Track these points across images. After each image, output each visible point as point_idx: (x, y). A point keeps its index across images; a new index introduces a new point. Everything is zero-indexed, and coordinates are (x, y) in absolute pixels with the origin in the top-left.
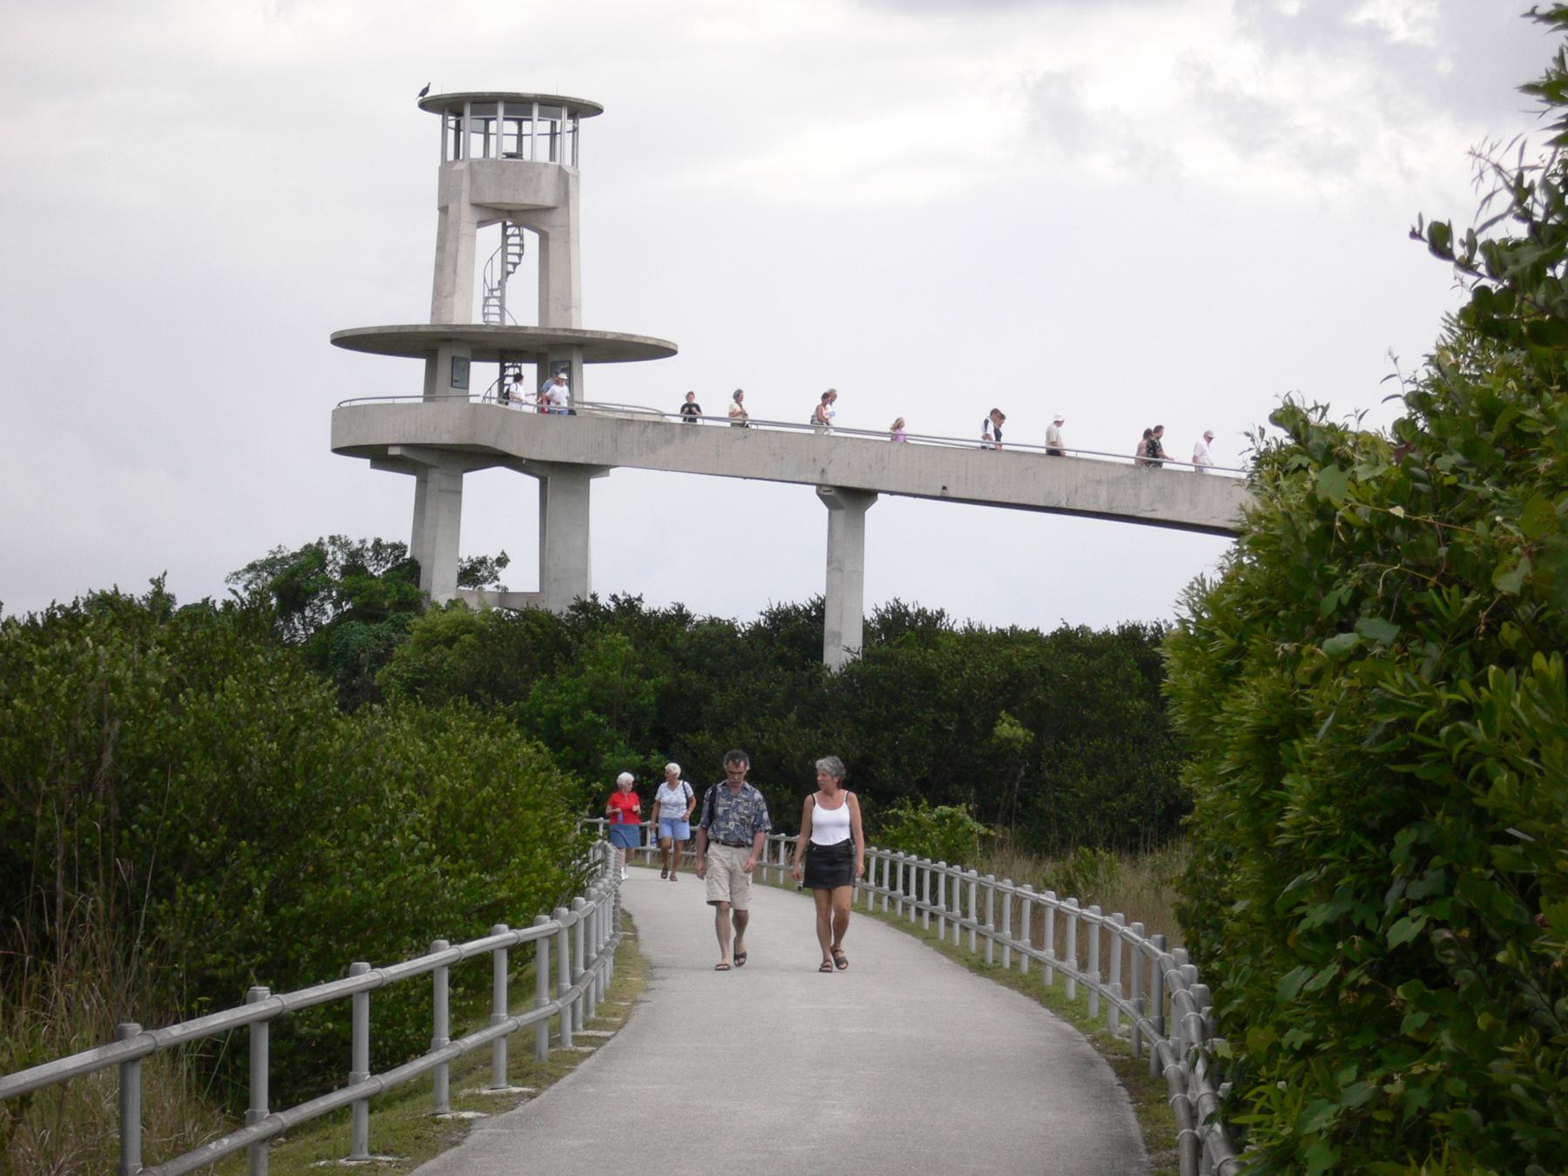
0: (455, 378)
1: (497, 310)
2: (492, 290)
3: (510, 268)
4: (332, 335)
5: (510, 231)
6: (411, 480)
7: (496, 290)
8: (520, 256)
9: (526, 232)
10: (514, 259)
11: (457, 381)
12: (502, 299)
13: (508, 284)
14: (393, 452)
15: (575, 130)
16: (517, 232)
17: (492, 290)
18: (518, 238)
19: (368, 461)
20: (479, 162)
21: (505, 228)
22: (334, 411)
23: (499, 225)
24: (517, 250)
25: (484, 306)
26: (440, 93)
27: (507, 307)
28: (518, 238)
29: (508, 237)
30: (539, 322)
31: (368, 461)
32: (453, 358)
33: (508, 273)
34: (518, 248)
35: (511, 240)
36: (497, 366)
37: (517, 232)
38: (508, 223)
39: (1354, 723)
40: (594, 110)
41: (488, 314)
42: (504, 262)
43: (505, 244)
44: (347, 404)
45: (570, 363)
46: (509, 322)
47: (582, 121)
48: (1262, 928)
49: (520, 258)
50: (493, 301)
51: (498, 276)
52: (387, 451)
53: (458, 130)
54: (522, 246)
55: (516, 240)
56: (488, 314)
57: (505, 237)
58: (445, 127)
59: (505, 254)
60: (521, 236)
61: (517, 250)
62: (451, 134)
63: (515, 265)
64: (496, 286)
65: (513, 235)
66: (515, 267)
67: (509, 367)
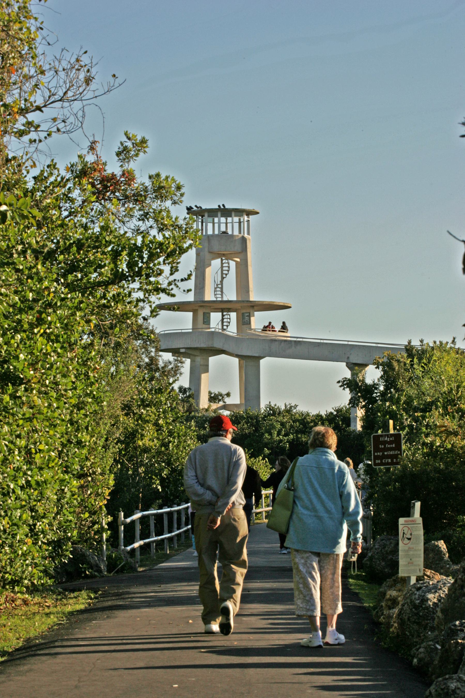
5: (224, 261)
8: (228, 271)
10: (226, 272)
12: (222, 288)
17: (217, 285)
21: (222, 260)
23: (220, 260)
24: (227, 268)
25: (215, 291)
33: (224, 278)
42: (222, 274)
43: (222, 267)
50: (218, 289)
51: (220, 279)
53: (202, 222)
54: (229, 267)
57: (222, 264)
59: (222, 270)
60: (228, 263)
63: (226, 274)
64: (219, 283)
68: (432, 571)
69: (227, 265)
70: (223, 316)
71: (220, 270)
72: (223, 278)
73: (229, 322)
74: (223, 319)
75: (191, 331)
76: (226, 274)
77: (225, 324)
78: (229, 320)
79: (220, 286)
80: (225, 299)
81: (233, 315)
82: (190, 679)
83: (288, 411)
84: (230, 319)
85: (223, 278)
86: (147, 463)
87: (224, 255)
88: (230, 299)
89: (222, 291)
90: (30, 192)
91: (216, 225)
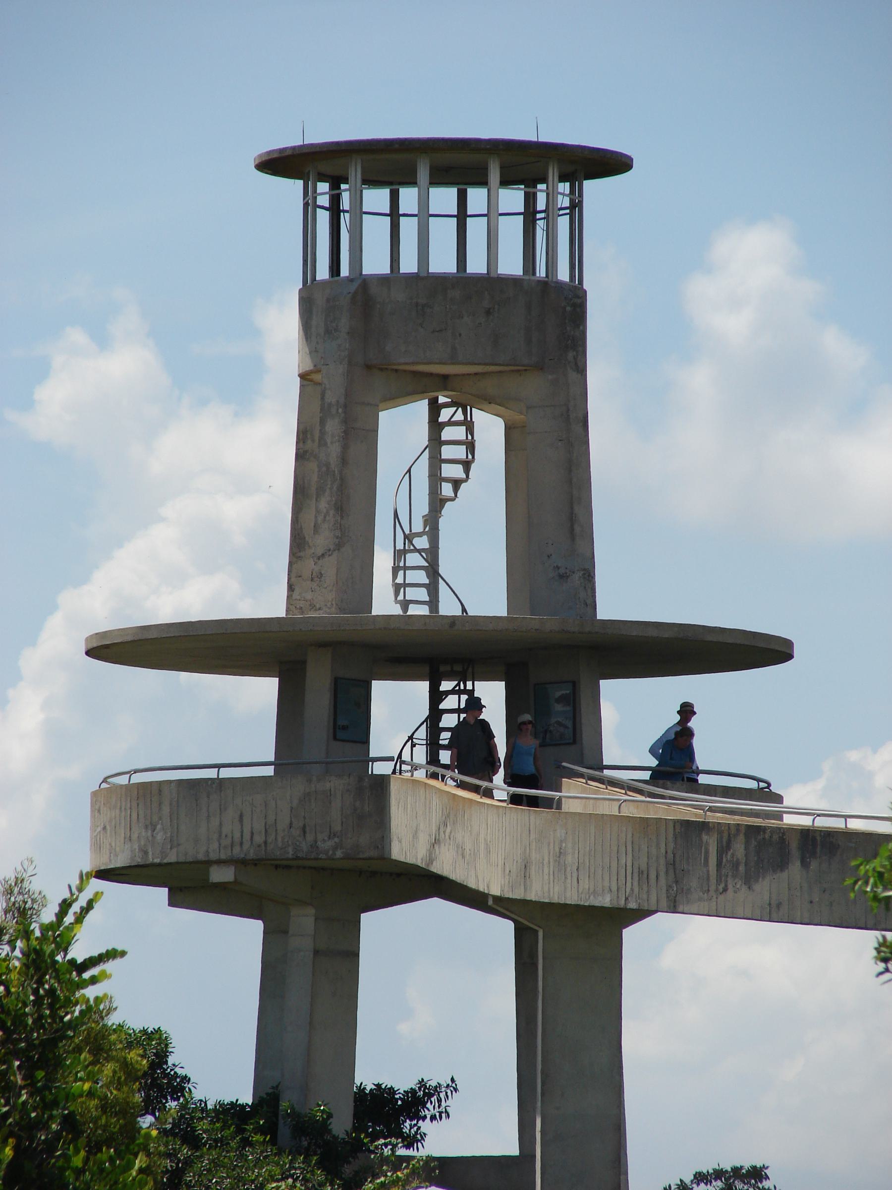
0: (341, 722)
1: (422, 577)
3: (447, 490)
4: (88, 640)
5: (445, 415)
6: (253, 929)
7: (419, 535)
8: (467, 465)
9: (480, 417)
11: (344, 728)
12: (432, 555)
13: (442, 523)
14: (221, 875)
15: (576, 206)
16: (459, 416)
17: (408, 538)
18: (463, 429)
19: (162, 893)
20: (382, 280)
21: (435, 409)
22: (94, 794)
23: (422, 407)
24: (460, 452)
25: (395, 570)
26: (298, 142)
27: (441, 571)
28: (463, 429)
29: (442, 426)
30: (509, 609)
31: (162, 893)
32: (337, 682)
33: (443, 501)
34: (460, 467)
35: (448, 434)
36: (424, 687)
37: (459, 416)
38: (442, 400)
39: (13, 912)
41: (405, 585)
42: (435, 479)
43: (436, 442)
44: (123, 780)
45: (574, 685)
46: (448, 607)
47: (589, 186)
48: (541, 204)
49: (467, 471)
50: (414, 559)
51: (422, 507)
52: (207, 874)
53: (335, 210)
54: (471, 446)
55: (459, 433)
56: (405, 585)
57: (435, 426)
58: (309, 207)
59: (436, 462)
60: (469, 426)
61: (460, 452)
62: (323, 218)
63: (457, 484)
64: (418, 526)
65: (450, 423)
66: (456, 488)
67: (447, 693)
72: (437, 503)
75: (269, 771)
85: (437, 503)
87: (444, 382)
89: (433, 571)
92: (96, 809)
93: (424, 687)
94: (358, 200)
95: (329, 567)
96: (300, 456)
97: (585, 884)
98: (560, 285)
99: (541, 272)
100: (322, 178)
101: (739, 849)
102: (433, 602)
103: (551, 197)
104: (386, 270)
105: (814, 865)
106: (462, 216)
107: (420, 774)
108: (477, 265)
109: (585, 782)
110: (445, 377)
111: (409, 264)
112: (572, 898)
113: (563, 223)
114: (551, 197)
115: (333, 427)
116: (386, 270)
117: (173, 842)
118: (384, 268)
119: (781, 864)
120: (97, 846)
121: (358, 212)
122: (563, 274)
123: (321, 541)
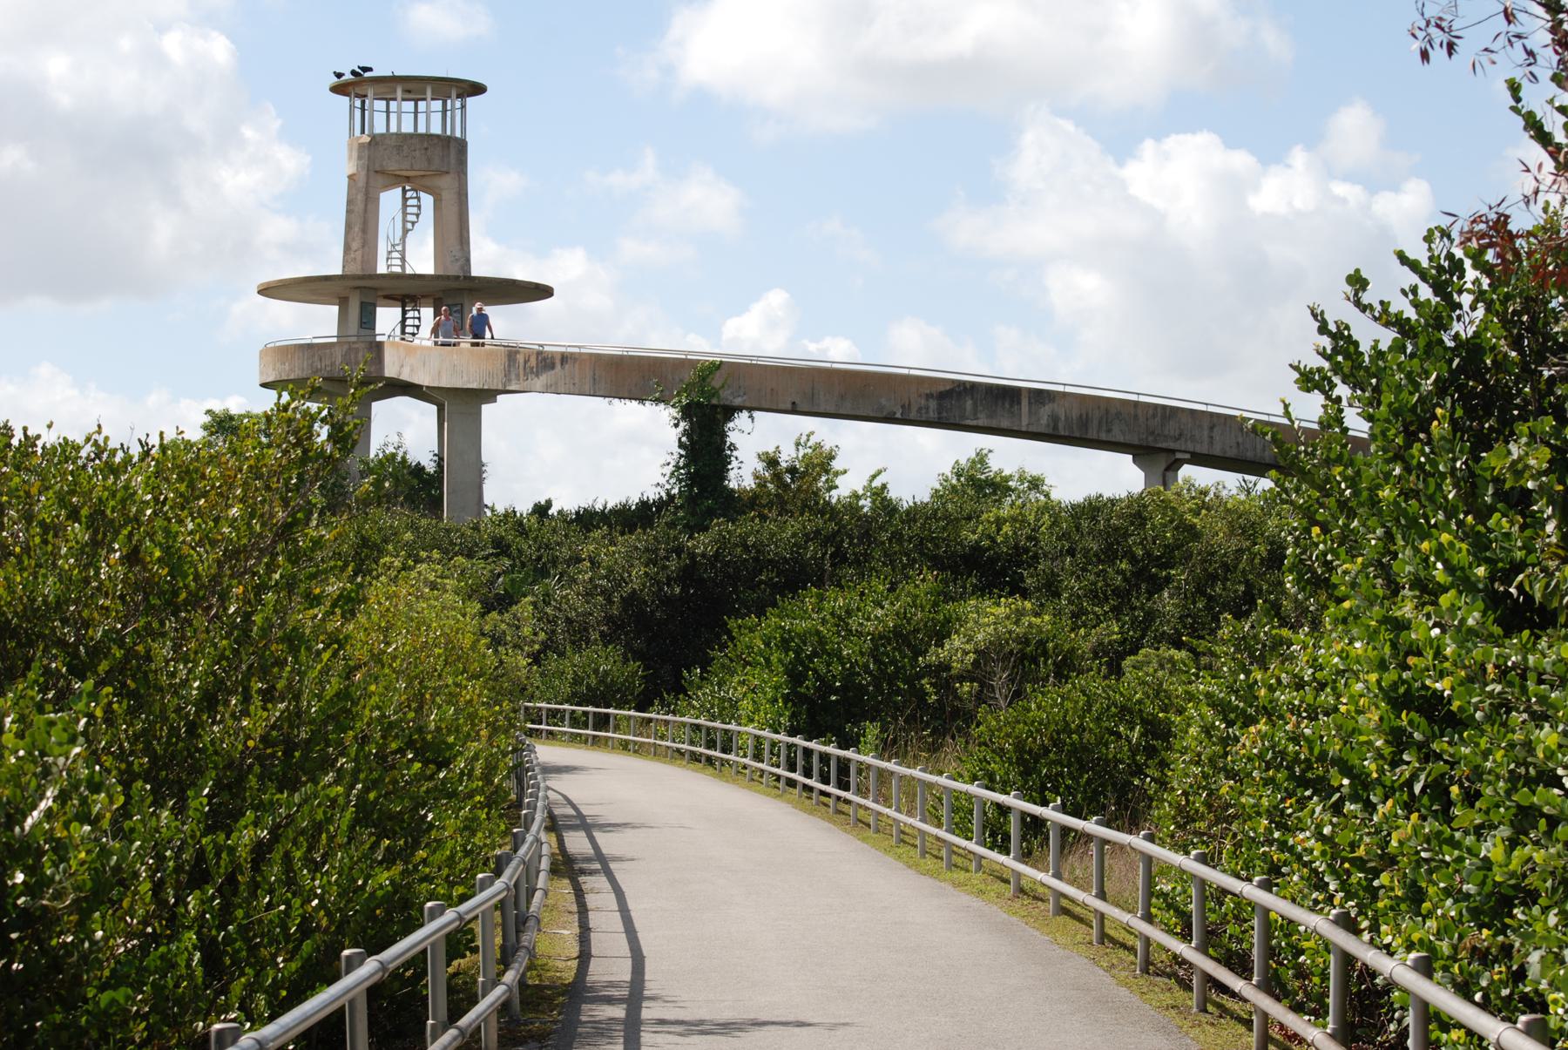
2: (393, 246)
3: (409, 226)
5: (409, 194)
9: (422, 195)
10: (413, 218)
15: (463, 107)
17: (393, 246)
21: (404, 191)
23: (399, 190)
24: (415, 210)
32: (362, 303)
33: (408, 230)
40: (477, 89)
42: (405, 221)
43: (405, 206)
48: (449, 107)
50: (395, 255)
51: (399, 233)
53: (363, 109)
54: (419, 207)
55: (414, 202)
57: (405, 199)
58: (352, 107)
59: (405, 214)
60: (418, 199)
62: (358, 113)
63: (413, 223)
64: (397, 241)
68: (983, 477)
69: (415, 210)
70: (404, 313)
71: (400, 214)
72: (405, 231)
73: (418, 327)
74: (404, 320)
75: (335, 340)
76: (413, 223)
77: (409, 330)
78: (417, 322)
79: (399, 248)
80: (409, 271)
81: (427, 313)
82: (200, 980)
83: (541, 510)
84: (419, 319)
85: (405, 231)
86: (1369, 751)
87: (408, 179)
88: (418, 272)
90: (938, 677)
91: (393, 117)
92: (261, 358)
93: (399, 310)
94: (372, 105)
95: (359, 255)
96: (348, 212)
97: (465, 379)
98: (456, 139)
99: (449, 133)
100: (357, 96)
101: (533, 362)
102: (403, 267)
103: (453, 105)
104: (384, 131)
105: (567, 367)
106: (416, 112)
107: (397, 339)
108: (422, 129)
109: (954, 857)
110: (408, 177)
111: (393, 129)
112: (459, 384)
113: (458, 113)
114: (453, 105)
115: (360, 197)
116: (384, 131)
117: (292, 370)
118: (383, 130)
119: (553, 367)
120: (261, 373)
121: (372, 111)
122: (458, 134)
123: (355, 245)
